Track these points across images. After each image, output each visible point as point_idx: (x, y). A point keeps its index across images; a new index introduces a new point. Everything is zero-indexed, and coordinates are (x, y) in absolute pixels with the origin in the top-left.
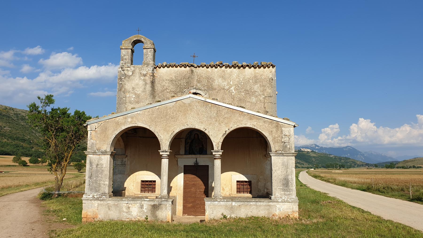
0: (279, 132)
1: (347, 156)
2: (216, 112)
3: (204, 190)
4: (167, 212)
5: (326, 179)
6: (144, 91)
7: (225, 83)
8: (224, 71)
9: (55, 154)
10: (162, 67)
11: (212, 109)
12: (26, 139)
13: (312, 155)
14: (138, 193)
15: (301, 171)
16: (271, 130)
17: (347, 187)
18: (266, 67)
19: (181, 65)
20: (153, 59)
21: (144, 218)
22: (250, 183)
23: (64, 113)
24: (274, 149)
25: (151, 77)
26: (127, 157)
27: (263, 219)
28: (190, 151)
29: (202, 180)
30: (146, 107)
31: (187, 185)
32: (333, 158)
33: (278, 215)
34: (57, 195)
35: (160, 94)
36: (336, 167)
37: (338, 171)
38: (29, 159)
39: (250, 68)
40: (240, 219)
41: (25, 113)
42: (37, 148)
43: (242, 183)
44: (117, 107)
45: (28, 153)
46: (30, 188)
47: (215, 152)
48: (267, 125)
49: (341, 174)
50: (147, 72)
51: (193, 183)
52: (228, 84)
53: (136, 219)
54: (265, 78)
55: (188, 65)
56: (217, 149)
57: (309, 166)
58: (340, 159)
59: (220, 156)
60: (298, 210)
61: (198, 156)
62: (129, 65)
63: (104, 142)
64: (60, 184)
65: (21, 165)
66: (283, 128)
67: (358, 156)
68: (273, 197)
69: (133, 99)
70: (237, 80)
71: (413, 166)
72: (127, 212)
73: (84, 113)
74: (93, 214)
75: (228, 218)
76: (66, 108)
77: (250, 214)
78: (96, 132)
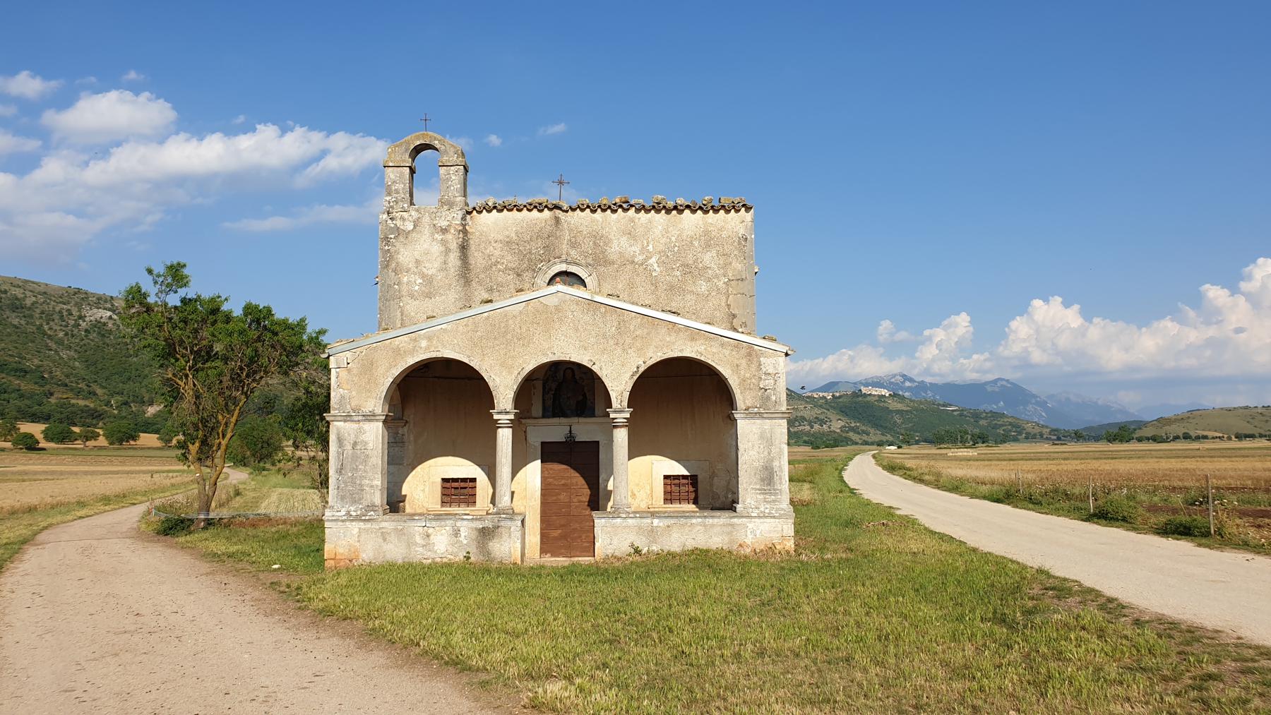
0: (754, 367)
1: (995, 407)
2: (615, 324)
3: (588, 497)
4: (512, 542)
5: (916, 475)
6: (444, 267)
7: (636, 249)
8: (632, 220)
9: (195, 419)
10: (484, 210)
11: (608, 318)
12: (28, 370)
13: (894, 405)
14: (436, 507)
15: (858, 452)
16: (736, 362)
17: (962, 493)
18: (731, 210)
19: (531, 205)
20: (463, 192)
21: (462, 557)
22: (693, 480)
23: (214, 310)
24: (743, 403)
25: (459, 234)
26: (407, 426)
27: (719, 553)
28: (555, 410)
29: (582, 476)
30: (460, 314)
31: (550, 488)
32: (955, 413)
33: (750, 544)
34: (203, 524)
35: (482, 276)
36: (963, 442)
37: (965, 452)
38: (43, 429)
39: (694, 212)
40: (669, 553)
41: (20, 287)
42: (65, 396)
43: (677, 481)
44: (380, 308)
45: (36, 409)
46: (97, 511)
47: (615, 412)
48: (727, 352)
49: (969, 460)
50: (448, 223)
51: (563, 482)
52: (643, 250)
53: (445, 560)
54: (729, 236)
55: (546, 206)
56: (619, 406)
57: (884, 438)
58: (976, 416)
59: (626, 421)
60: (793, 534)
61: (575, 420)
62: (406, 205)
63: (369, 394)
64: (211, 494)
65: (21, 446)
66: (761, 359)
67: (1030, 407)
68: (739, 507)
69: (417, 288)
70: (663, 240)
71: (1184, 434)
72: (423, 546)
73: (269, 312)
74: (350, 550)
75: (643, 552)
76: (219, 297)
77: (690, 545)
78: (349, 371)
